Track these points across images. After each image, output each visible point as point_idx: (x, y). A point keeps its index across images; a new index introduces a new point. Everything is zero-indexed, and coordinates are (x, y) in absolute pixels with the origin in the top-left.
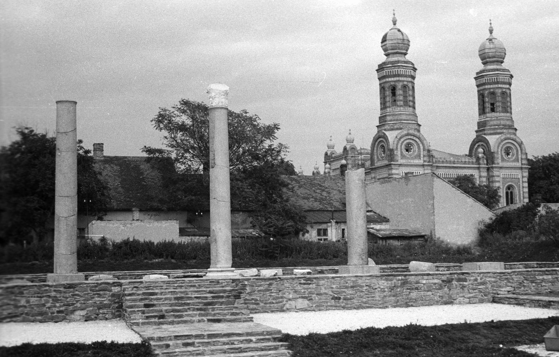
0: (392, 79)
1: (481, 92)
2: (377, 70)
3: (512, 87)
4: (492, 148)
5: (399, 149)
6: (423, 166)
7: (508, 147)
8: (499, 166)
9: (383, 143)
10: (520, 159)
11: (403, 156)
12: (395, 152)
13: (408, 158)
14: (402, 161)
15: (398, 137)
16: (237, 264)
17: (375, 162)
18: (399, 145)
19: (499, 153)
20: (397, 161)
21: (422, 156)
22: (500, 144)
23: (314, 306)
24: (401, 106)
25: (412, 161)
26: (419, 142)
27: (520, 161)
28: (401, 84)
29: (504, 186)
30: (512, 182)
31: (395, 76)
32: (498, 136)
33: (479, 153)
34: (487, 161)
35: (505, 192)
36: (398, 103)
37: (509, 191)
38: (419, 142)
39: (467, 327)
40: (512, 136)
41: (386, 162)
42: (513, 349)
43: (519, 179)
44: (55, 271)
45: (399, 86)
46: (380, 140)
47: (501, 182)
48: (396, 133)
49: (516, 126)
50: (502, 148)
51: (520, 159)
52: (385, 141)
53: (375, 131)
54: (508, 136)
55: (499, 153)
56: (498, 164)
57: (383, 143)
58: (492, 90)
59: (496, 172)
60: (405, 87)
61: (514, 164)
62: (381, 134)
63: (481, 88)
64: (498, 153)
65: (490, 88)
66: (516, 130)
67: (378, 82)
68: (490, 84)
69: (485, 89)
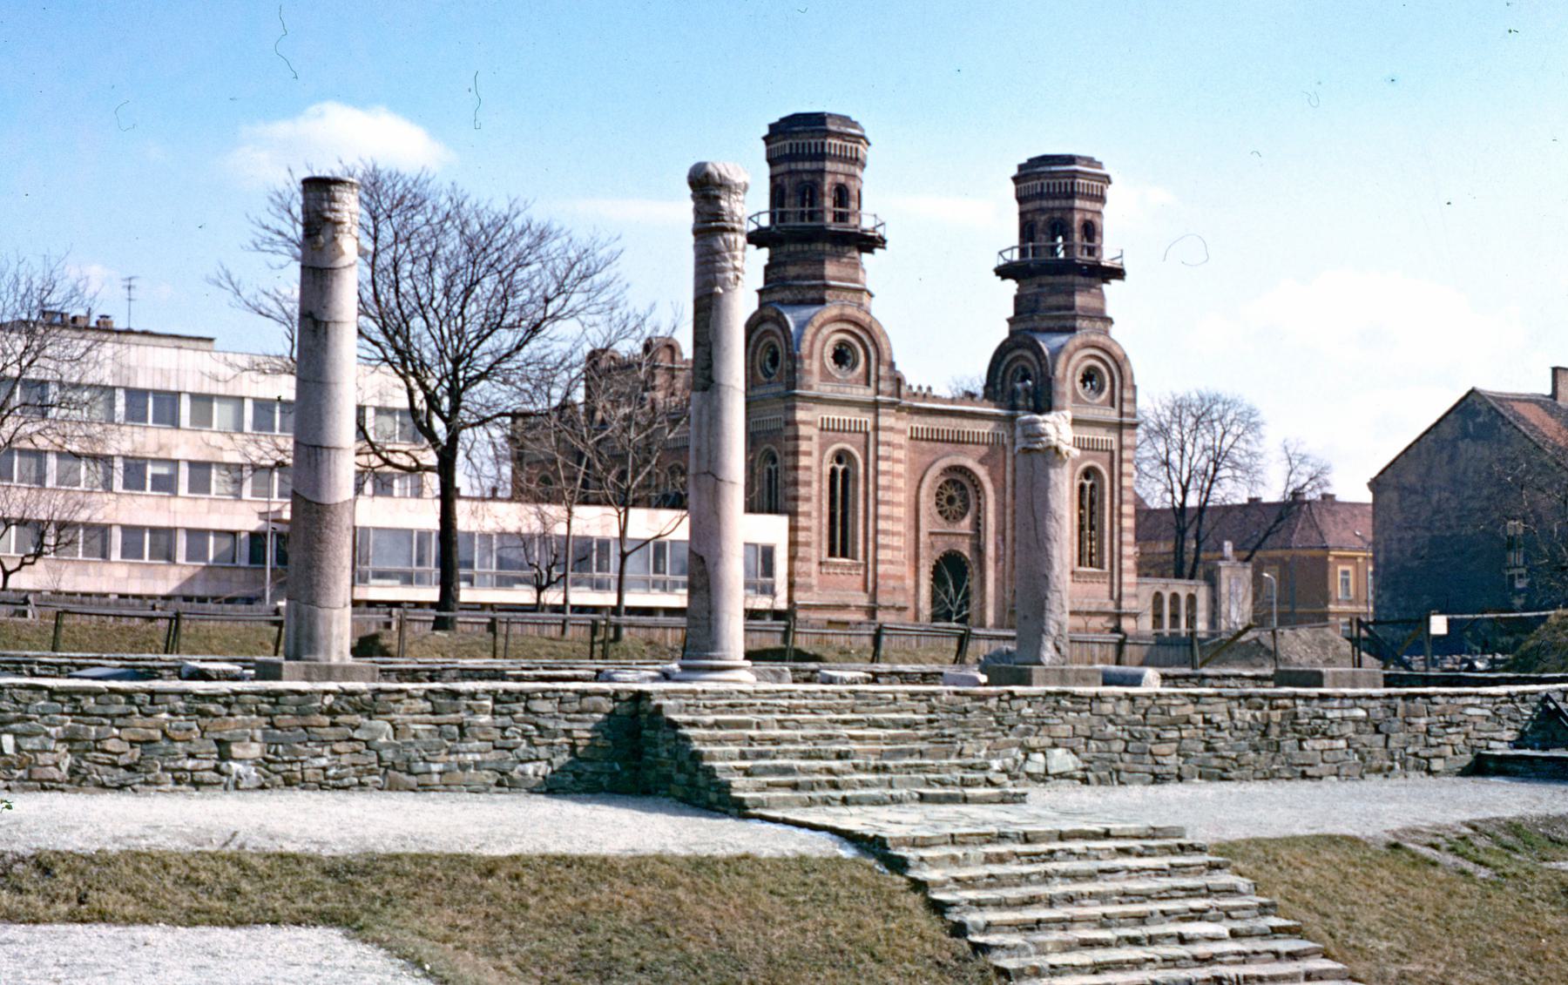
1: (1029, 216)
2: (765, 138)
3: (1107, 210)
7: (842, 343)
9: (772, 338)
11: (826, 376)
12: (807, 362)
13: (839, 381)
23: (996, 764)
27: (873, 384)
30: (1093, 458)
34: (1035, 402)
35: (827, 470)
37: (840, 468)
39: (599, 869)
40: (1101, 339)
49: (1109, 313)
50: (1075, 369)
52: (779, 332)
54: (1094, 338)
57: (772, 338)
58: (1057, 215)
63: (782, 168)
65: (1053, 209)
66: (1110, 321)
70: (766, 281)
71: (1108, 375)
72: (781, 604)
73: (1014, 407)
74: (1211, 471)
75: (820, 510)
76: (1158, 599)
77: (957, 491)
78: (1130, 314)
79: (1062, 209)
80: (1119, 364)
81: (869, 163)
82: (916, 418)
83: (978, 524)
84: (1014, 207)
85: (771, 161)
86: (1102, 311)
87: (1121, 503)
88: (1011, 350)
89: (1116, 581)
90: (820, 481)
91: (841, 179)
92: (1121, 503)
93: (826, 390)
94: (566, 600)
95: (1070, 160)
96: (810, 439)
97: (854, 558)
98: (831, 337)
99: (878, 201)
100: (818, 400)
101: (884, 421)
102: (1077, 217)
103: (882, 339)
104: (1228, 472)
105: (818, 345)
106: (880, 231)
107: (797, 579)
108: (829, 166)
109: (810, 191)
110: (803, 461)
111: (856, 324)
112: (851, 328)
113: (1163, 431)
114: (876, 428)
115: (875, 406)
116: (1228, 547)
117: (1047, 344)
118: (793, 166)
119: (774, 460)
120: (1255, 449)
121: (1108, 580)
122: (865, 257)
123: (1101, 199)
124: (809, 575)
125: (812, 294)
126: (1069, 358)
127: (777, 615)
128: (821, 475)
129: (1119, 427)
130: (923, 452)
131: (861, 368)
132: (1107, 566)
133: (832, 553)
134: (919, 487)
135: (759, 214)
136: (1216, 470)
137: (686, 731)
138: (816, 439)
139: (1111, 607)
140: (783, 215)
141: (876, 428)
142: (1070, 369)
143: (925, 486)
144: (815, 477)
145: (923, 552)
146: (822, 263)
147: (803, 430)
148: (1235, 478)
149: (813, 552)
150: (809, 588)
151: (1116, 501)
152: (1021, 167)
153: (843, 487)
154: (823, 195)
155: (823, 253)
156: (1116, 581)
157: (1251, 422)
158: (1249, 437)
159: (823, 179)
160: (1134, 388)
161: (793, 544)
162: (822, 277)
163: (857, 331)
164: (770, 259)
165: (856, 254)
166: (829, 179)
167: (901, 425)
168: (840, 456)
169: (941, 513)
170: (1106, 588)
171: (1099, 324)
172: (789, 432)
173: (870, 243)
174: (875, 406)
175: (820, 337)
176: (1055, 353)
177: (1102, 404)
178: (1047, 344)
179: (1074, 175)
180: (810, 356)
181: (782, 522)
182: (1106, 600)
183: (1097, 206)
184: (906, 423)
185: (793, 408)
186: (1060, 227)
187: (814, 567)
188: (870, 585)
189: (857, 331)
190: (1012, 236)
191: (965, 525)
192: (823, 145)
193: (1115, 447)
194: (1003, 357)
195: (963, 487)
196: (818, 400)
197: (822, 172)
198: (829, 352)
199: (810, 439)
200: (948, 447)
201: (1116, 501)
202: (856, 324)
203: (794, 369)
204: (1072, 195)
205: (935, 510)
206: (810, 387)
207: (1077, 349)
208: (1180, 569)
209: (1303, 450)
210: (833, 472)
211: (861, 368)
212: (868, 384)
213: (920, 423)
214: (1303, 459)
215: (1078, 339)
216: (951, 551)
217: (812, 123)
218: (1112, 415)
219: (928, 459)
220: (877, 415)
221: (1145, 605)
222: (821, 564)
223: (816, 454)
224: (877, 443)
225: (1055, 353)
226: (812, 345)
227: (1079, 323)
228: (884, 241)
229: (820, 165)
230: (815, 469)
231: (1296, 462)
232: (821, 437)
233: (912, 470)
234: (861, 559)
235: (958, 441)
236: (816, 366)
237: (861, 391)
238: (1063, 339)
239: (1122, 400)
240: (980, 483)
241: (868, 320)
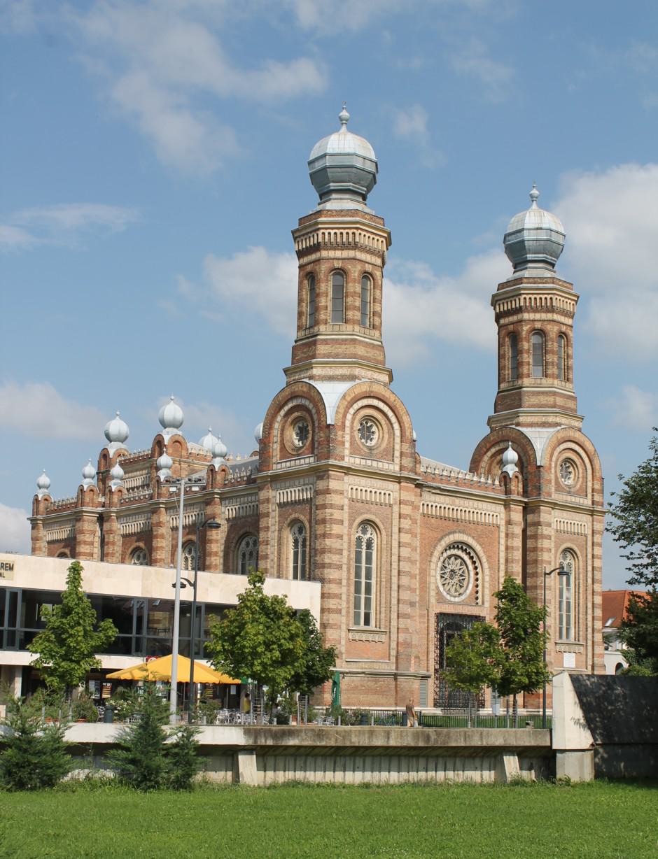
0: (338, 254)
4: (538, 458)
5: (348, 430)
6: (399, 480)
10: (589, 490)
12: (340, 433)
14: (352, 460)
15: (349, 399)
17: (274, 460)
18: (349, 417)
19: (553, 471)
20: (342, 458)
21: (397, 454)
22: (554, 449)
24: (354, 322)
26: (393, 419)
28: (359, 267)
29: (557, 547)
31: (344, 247)
32: (551, 430)
33: (113, 478)
34: (525, 487)
36: (350, 314)
38: (393, 419)
41: (308, 461)
42: (120, 632)
43: (586, 536)
45: (355, 271)
48: (343, 387)
51: (589, 490)
53: (282, 381)
55: (553, 471)
59: (546, 515)
60: (367, 276)
61: (577, 500)
62: (298, 388)
64: (550, 468)
65: (534, 321)
67: (295, 263)
68: (536, 310)
100: (348, 471)
196: (348, 471)
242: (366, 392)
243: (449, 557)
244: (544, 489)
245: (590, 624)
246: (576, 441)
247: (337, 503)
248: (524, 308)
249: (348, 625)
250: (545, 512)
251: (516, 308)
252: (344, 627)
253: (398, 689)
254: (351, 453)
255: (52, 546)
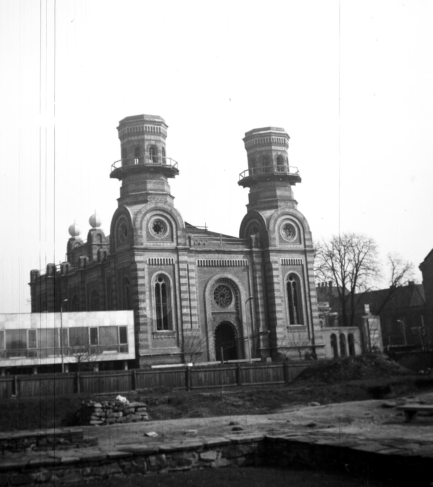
3: (289, 151)
5: (144, 228)
7: (158, 221)
8: (143, 247)
11: (150, 238)
12: (139, 231)
13: (157, 240)
14: (148, 244)
16: (253, 357)
25: (162, 244)
27: (175, 240)
29: (150, 274)
30: (294, 269)
40: (291, 210)
44: (240, 353)
46: (121, 219)
47: (280, 270)
54: (287, 210)
56: (142, 244)
58: (264, 154)
61: (295, 246)
63: (253, 151)
69: (256, 152)
70: (121, 194)
71: (297, 227)
72: (131, 355)
73: (251, 247)
74: (355, 272)
75: (151, 306)
76: (333, 336)
77: (225, 291)
78: (305, 198)
79: (138, 140)
80: (302, 221)
81: (289, 145)
82: (200, 255)
83: (238, 306)
84: (118, 143)
85: (247, 148)
86: (291, 197)
87: (309, 291)
88: (249, 220)
89: (311, 330)
90: (150, 291)
91: (153, 143)
92: (309, 291)
93: (150, 245)
94: (62, 362)
95: (269, 128)
96: (143, 270)
97: (171, 329)
98: (281, 222)
99: (296, 161)
100: (146, 250)
101: (182, 258)
102: (274, 154)
103: (178, 218)
104: (364, 271)
105: (144, 223)
106: (176, 167)
107: (140, 343)
108: (146, 137)
109: (138, 151)
110: (140, 281)
111: (164, 211)
112: (161, 213)
113: (331, 255)
114: (178, 262)
115: (176, 251)
116: (367, 308)
117: (266, 214)
118: (130, 139)
119: (129, 283)
120: (375, 259)
121: (307, 330)
122: (169, 180)
123: (286, 145)
124: (146, 340)
125: (141, 199)
126: (276, 220)
127: (130, 363)
128: (150, 288)
129: (304, 252)
130: (205, 273)
131: (168, 233)
132: (305, 324)
133: (292, 322)
134: (205, 290)
135: (244, 172)
136: (357, 271)
137: (111, 429)
138: (146, 270)
139: (310, 344)
140: (254, 170)
141: (178, 262)
142: (277, 226)
143: (207, 289)
144: (147, 289)
145: (209, 324)
146: (275, 190)
147: (139, 266)
148: (366, 274)
149: (149, 328)
150: (147, 347)
151: (307, 290)
152: (246, 134)
153: (162, 291)
154: (144, 150)
155: (275, 186)
156: (311, 330)
157: (370, 246)
158: (371, 253)
159: (144, 143)
160: (310, 233)
161: (137, 325)
162: (145, 189)
163: (165, 214)
164: (123, 184)
165: (163, 178)
166: (147, 143)
167: (192, 260)
168: (161, 277)
169: (217, 303)
170: (307, 333)
171: (289, 204)
172: (132, 268)
173: (295, 179)
174: (176, 251)
175: (146, 219)
176: (269, 220)
177: (295, 242)
178: (266, 214)
179: (270, 134)
180: (141, 228)
181: (131, 313)
182: (307, 340)
183: (283, 148)
184: (194, 259)
185: (133, 255)
186: (267, 159)
187: (149, 336)
188: (181, 342)
189: (165, 214)
190: (245, 166)
191: (232, 307)
192: (143, 127)
193: (304, 263)
194: (246, 224)
195: (228, 289)
196: (146, 250)
197: (143, 140)
198: (151, 225)
199: (143, 270)
200: (218, 269)
201: (307, 290)
202: (164, 211)
203: (133, 236)
204: (143, 133)
205: (214, 301)
206: (275, 246)
207: (279, 216)
208: (344, 321)
209: (398, 257)
210: (157, 286)
211: (168, 233)
212: (301, 243)
213: (202, 258)
214: (399, 262)
215: (280, 211)
216: (224, 321)
217: (139, 120)
218: (301, 247)
219: (208, 276)
220: (178, 256)
221: (326, 341)
222: (153, 334)
223: (147, 277)
224: (179, 270)
225: (269, 220)
226: (141, 222)
227: (279, 204)
228: (178, 171)
229: (142, 137)
230: (147, 285)
231: (395, 264)
232: (149, 268)
233: (200, 283)
234: (305, 324)
235: (223, 265)
236: (144, 233)
237: (169, 244)
238: (272, 211)
239: (305, 239)
240: (237, 286)
241: (170, 209)
242: (153, 208)
243: (224, 286)
244: (272, 242)
245: (309, 314)
246: (291, 214)
247: (140, 268)
248: (145, 132)
249: (152, 329)
250: (273, 256)
251: (140, 131)
252: (150, 332)
253: (288, 346)
254: (280, 242)
255: (337, 289)
